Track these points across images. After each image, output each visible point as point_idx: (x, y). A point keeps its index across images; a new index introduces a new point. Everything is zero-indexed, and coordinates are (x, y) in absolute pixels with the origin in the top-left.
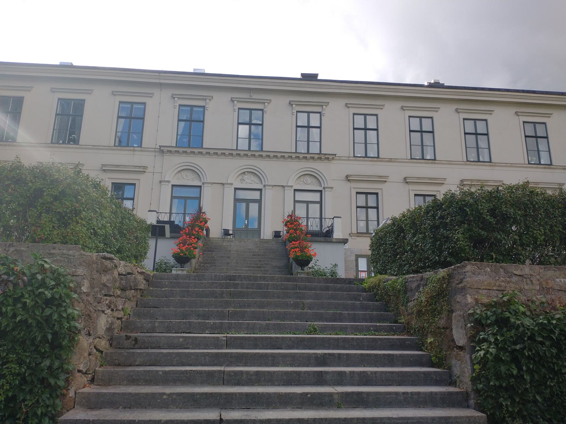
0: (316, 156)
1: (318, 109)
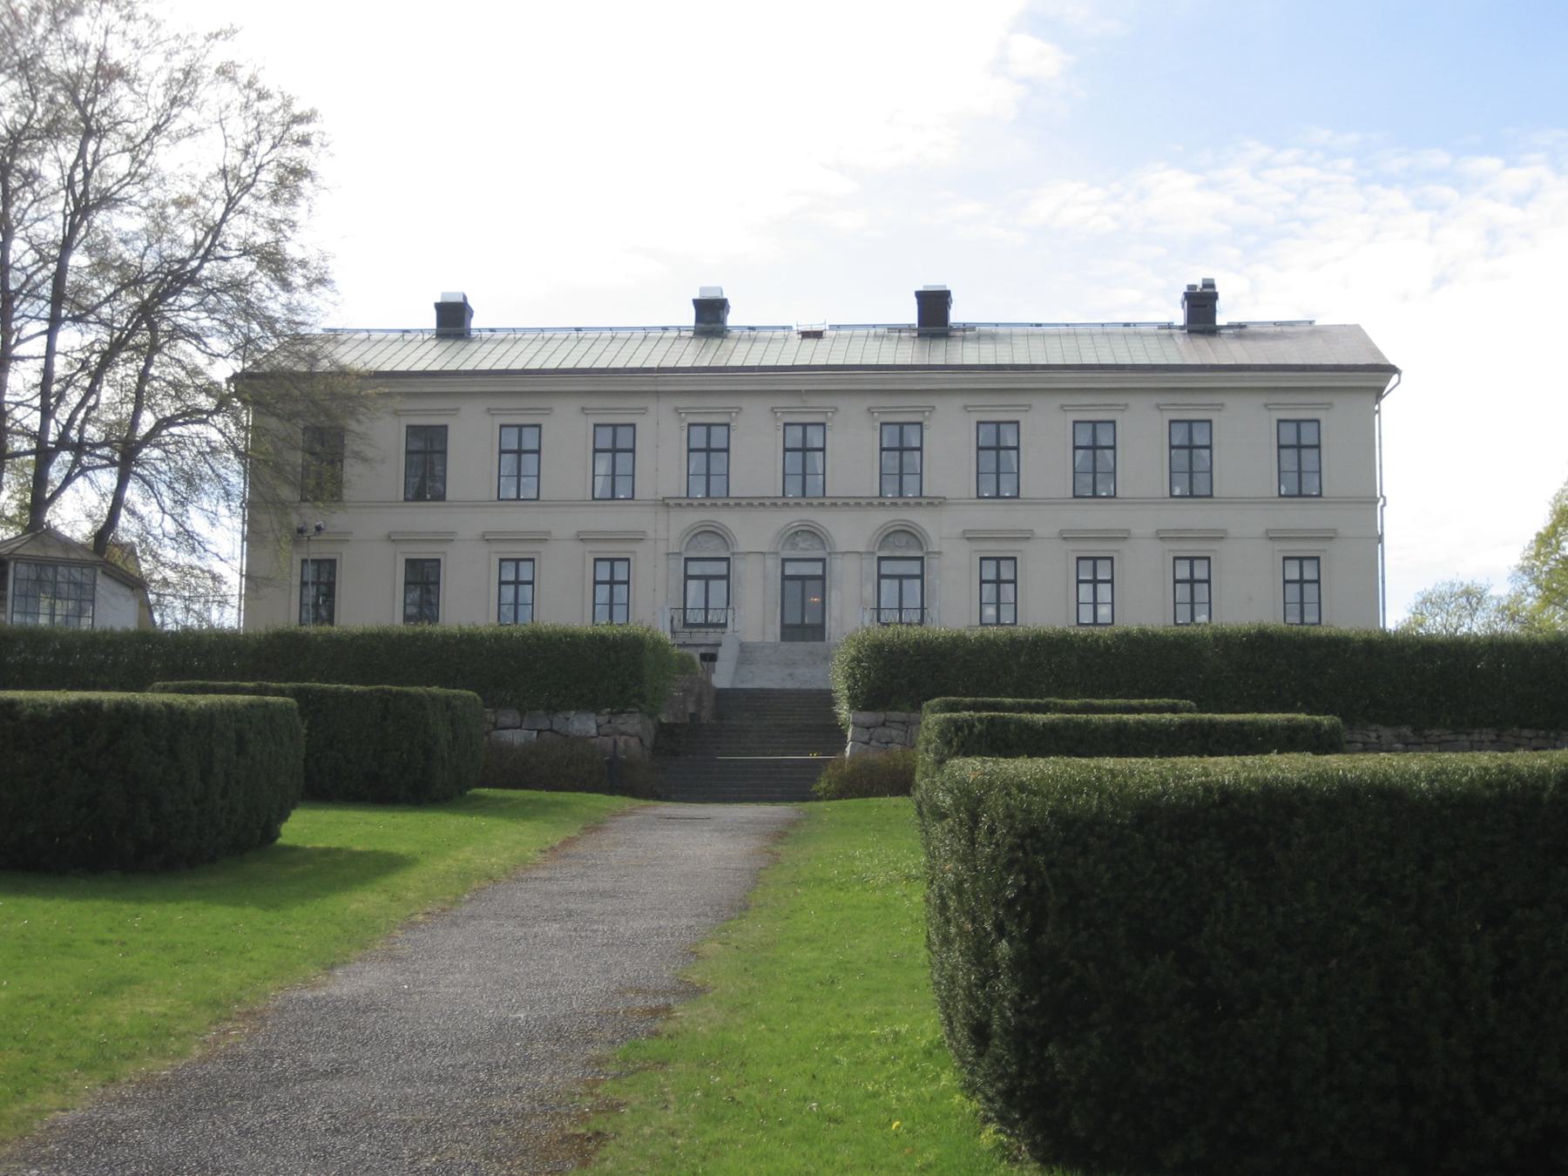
0: (875, 502)
1: (723, 419)
